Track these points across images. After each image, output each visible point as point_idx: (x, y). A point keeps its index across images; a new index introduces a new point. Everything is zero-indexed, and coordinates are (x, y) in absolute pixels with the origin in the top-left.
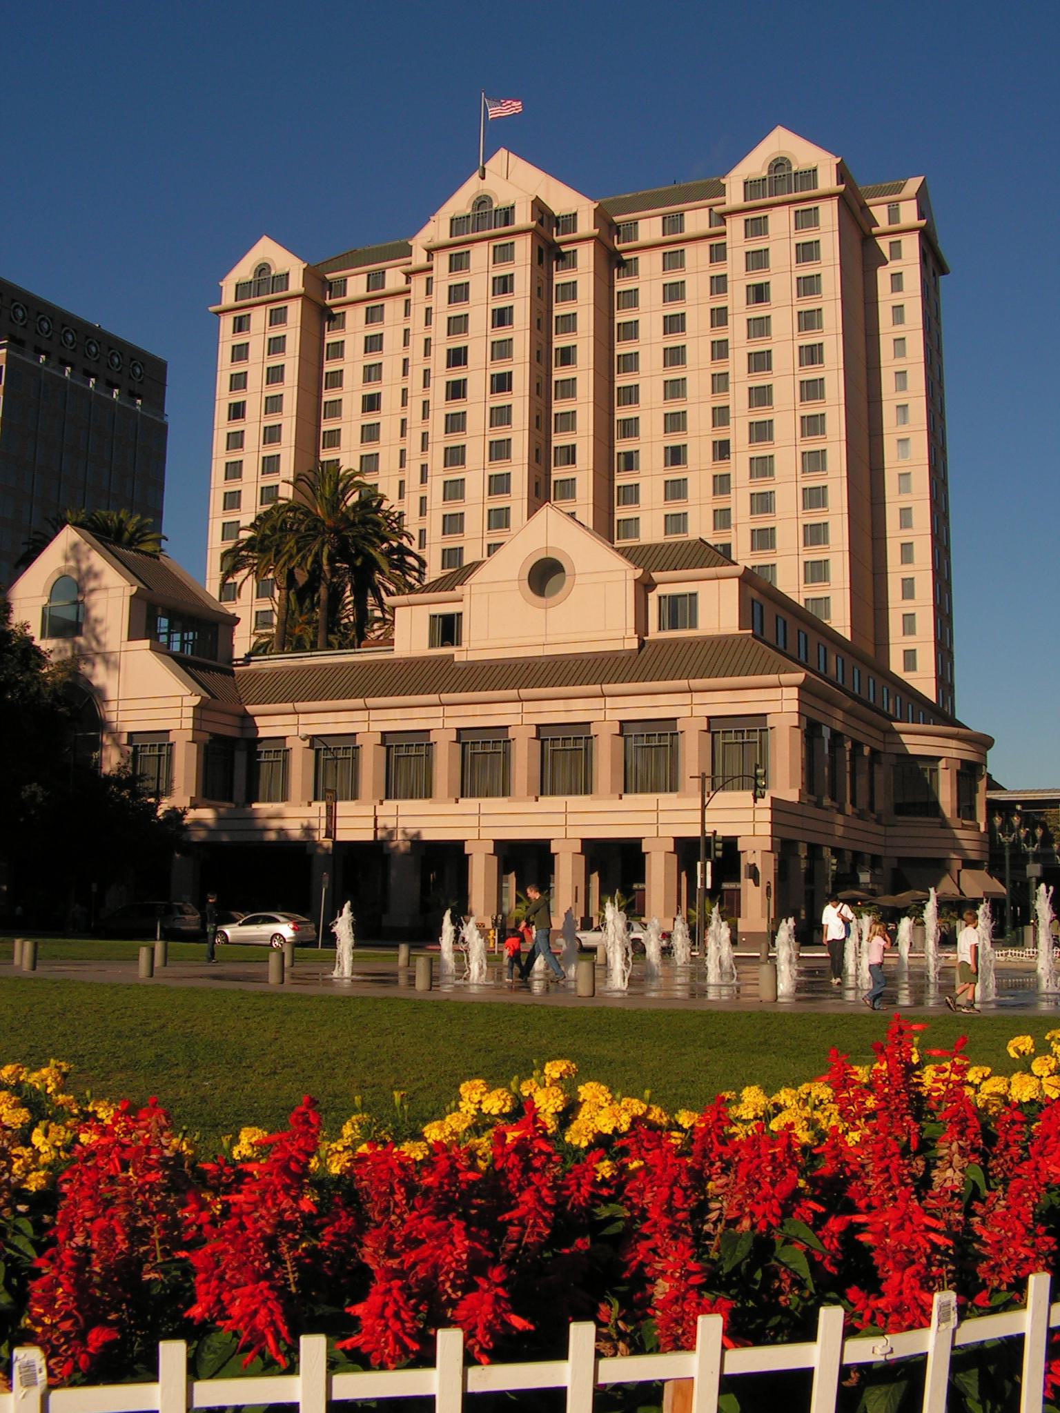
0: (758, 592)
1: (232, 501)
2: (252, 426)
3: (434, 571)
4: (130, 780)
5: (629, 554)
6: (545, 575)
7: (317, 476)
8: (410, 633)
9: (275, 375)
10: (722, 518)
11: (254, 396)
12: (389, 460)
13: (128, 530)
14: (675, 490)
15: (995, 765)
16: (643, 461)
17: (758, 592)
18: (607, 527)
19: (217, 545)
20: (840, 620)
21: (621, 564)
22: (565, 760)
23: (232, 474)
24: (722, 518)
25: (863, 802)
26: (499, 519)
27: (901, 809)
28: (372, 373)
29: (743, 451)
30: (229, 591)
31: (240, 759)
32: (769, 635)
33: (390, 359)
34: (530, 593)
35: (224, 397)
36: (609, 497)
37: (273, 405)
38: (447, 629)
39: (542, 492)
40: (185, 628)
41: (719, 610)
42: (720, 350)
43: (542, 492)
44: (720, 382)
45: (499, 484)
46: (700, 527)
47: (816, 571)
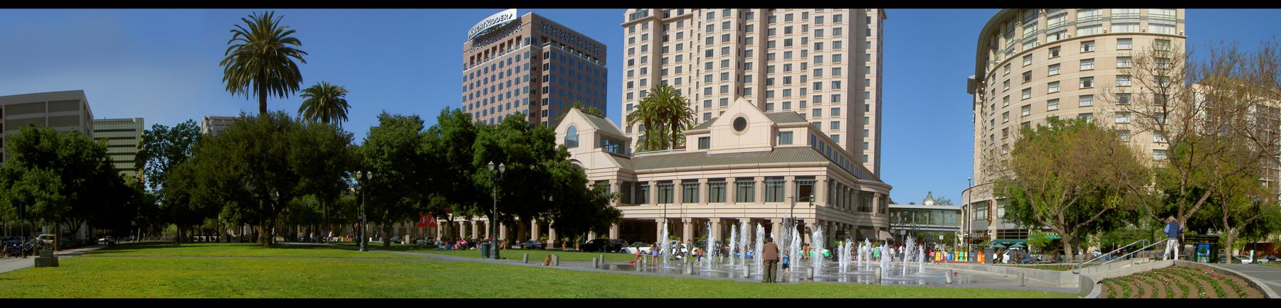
0: (814, 131)
1: (630, 96)
2: (637, 68)
3: (701, 121)
4: (596, 192)
5: (770, 117)
6: (740, 124)
7: (660, 85)
8: (692, 144)
9: (644, 48)
10: (803, 104)
11: (637, 57)
12: (685, 80)
13: (595, 105)
14: (787, 93)
15: (893, 195)
16: (776, 82)
17: (814, 131)
18: (765, 107)
19: (625, 113)
20: (842, 143)
21: (766, 119)
22: (745, 188)
23: (630, 87)
24: (803, 104)
25: (847, 206)
26: (724, 102)
27: (859, 209)
28: (679, 58)
29: (811, 68)
30: (629, 129)
31: (633, 189)
32: (818, 147)
33: (686, 42)
34: (733, 130)
35: (626, 58)
36: (765, 95)
37: (644, 60)
38: (704, 142)
39: (741, 92)
40: (612, 143)
41: (800, 138)
42: (805, 41)
43: (741, 92)
44: (804, 53)
45: (724, 89)
46: (795, 107)
47: (835, 125)
